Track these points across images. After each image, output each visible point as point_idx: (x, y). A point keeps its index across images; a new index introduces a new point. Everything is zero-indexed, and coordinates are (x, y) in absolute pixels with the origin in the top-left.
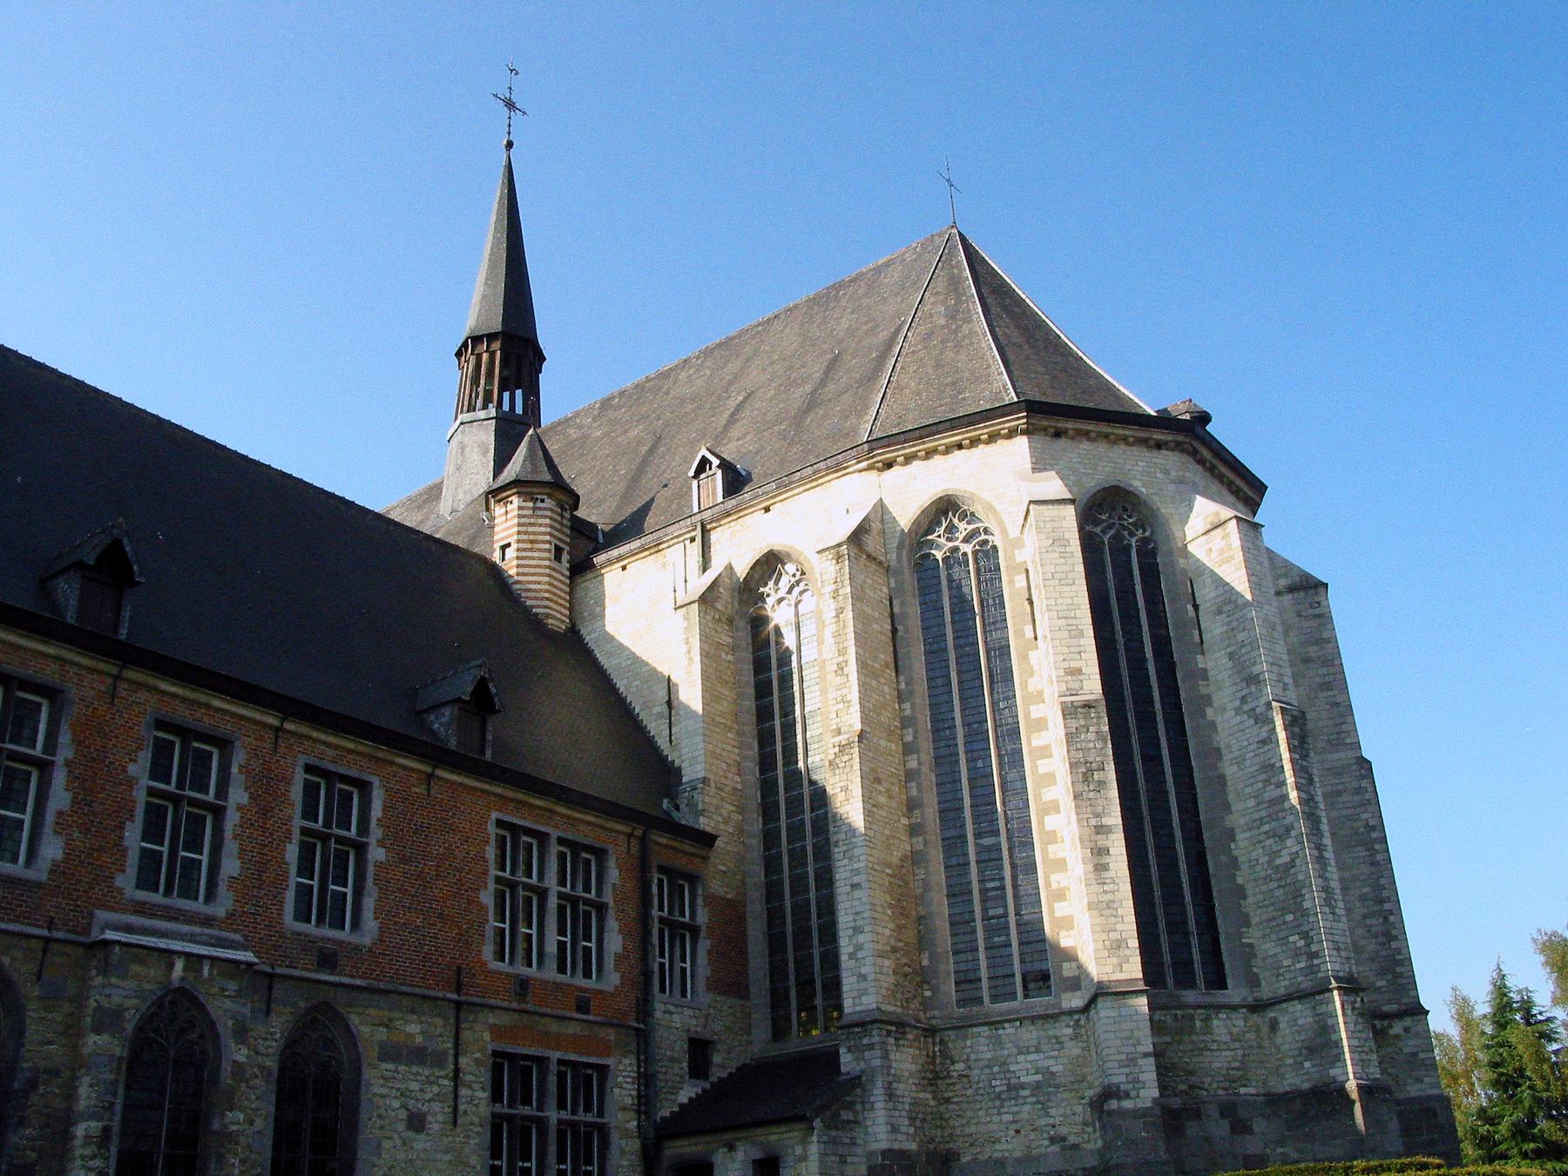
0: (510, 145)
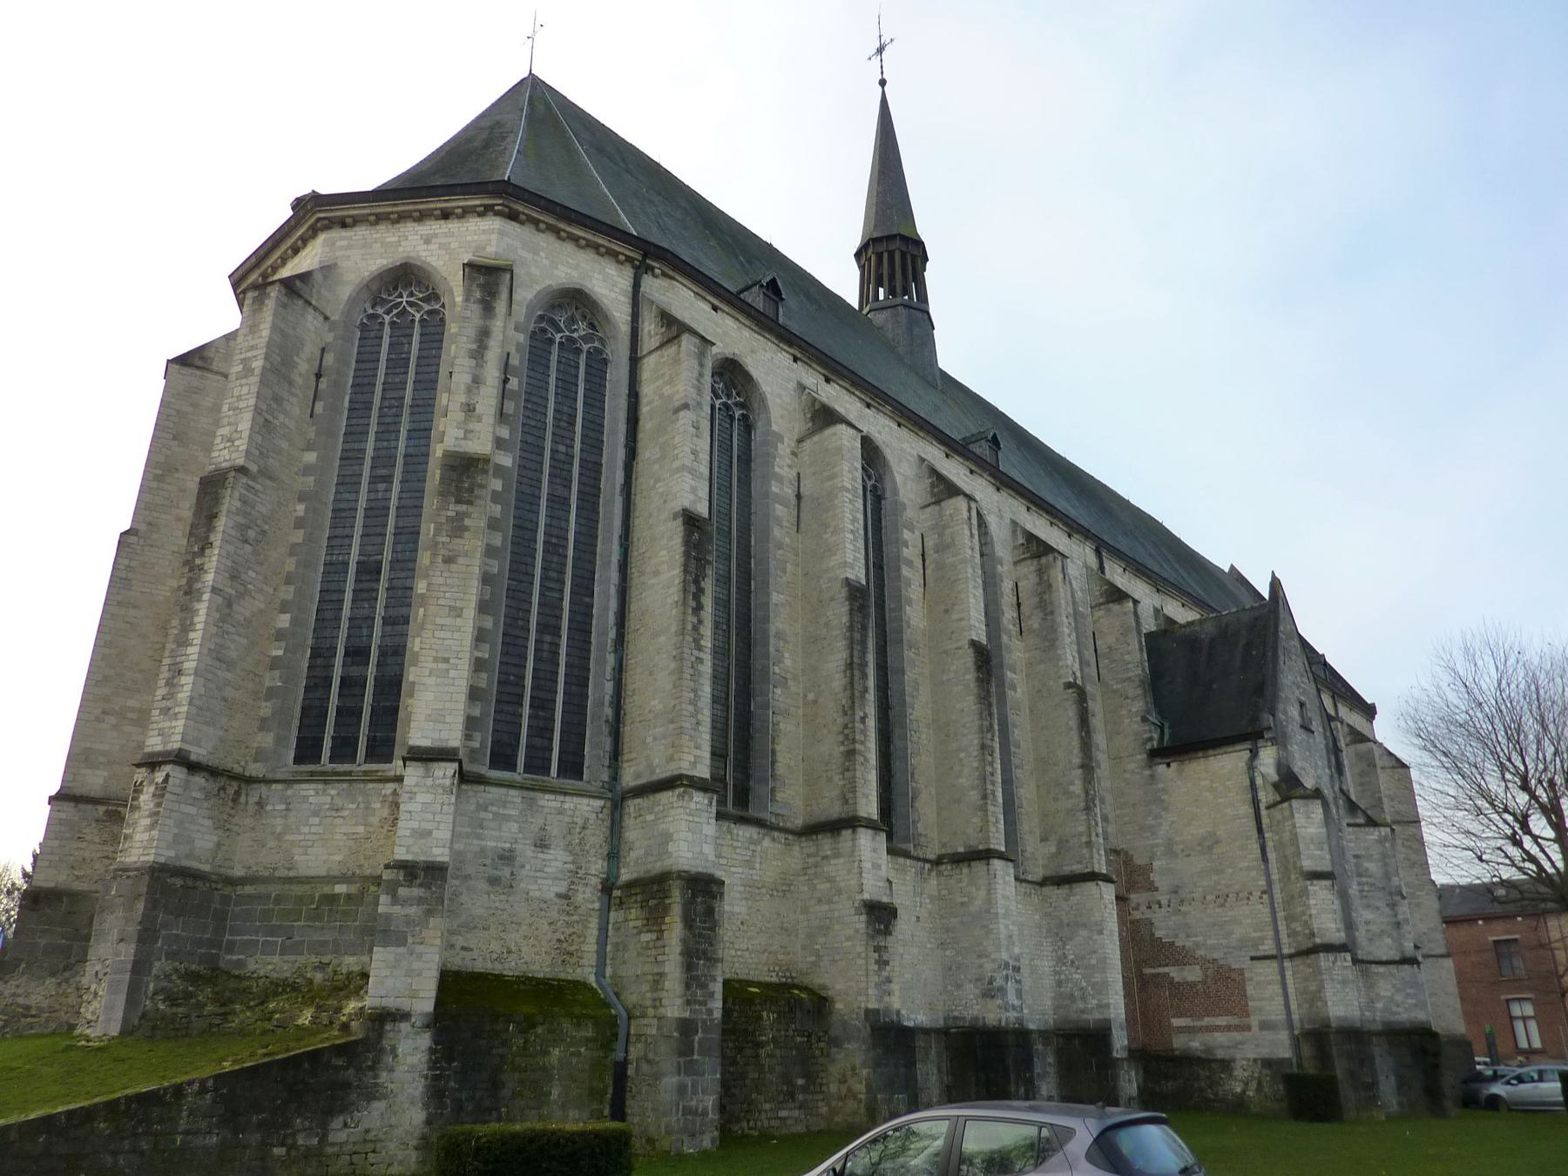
0: (883, 83)
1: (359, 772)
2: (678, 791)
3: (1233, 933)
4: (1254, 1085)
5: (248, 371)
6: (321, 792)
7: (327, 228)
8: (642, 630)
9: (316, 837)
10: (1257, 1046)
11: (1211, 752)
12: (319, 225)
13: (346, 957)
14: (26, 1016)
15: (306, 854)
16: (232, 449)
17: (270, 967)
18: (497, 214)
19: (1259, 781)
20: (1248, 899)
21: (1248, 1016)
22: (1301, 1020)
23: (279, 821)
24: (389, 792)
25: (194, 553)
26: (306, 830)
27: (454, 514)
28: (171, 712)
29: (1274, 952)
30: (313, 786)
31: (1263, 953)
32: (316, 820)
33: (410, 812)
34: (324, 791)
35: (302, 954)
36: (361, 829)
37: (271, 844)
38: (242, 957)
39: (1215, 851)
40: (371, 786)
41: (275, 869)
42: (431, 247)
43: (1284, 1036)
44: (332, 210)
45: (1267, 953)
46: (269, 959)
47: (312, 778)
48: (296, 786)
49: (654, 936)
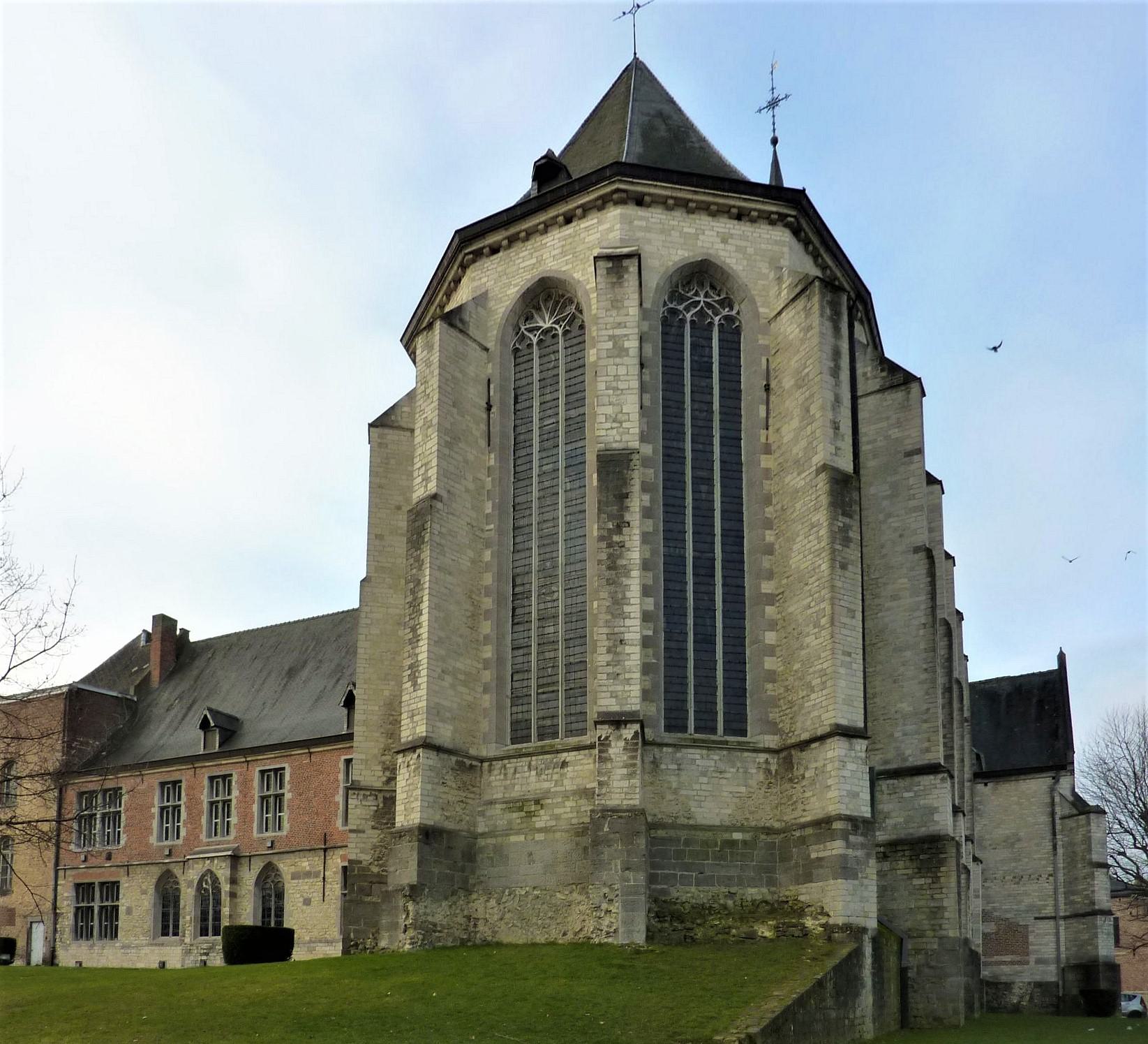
0: (775, 141)
1: (734, 742)
2: (940, 776)
3: (1023, 902)
4: (1028, 998)
5: (620, 351)
6: (705, 756)
7: (622, 202)
8: (879, 645)
9: (707, 794)
10: (1031, 974)
11: (1023, 777)
12: (615, 196)
13: (749, 889)
14: (435, 931)
15: (701, 807)
16: (621, 430)
17: (689, 895)
18: (787, 225)
19: (1057, 799)
20: (1038, 879)
21: (1028, 955)
22: (1067, 959)
23: (673, 779)
24: (762, 760)
25: (609, 530)
26: (697, 787)
27: (842, 525)
28: (621, 677)
29: (1053, 915)
30: (698, 751)
31: (1044, 915)
32: (705, 780)
33: (844, 777)
34: (708, 756)
35: (713, 885)
36: (743, 789)
37: (669, 797)
38: (665, 886)
39: (1016, 846)
40: (746, 754)
41: (676, 818)
42: (728, 247)
43: (1052, 968)
44: (632, 183)
45: (1049, 915)
46: (687, 888)
47: (709, 746)
48: (684, 751)
49: (930, 881)
